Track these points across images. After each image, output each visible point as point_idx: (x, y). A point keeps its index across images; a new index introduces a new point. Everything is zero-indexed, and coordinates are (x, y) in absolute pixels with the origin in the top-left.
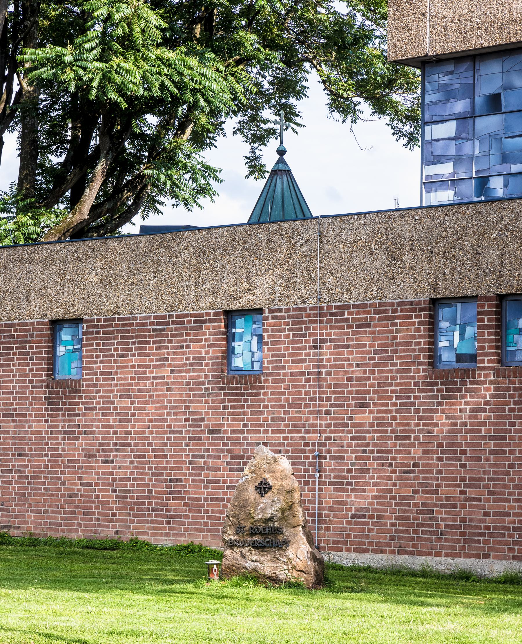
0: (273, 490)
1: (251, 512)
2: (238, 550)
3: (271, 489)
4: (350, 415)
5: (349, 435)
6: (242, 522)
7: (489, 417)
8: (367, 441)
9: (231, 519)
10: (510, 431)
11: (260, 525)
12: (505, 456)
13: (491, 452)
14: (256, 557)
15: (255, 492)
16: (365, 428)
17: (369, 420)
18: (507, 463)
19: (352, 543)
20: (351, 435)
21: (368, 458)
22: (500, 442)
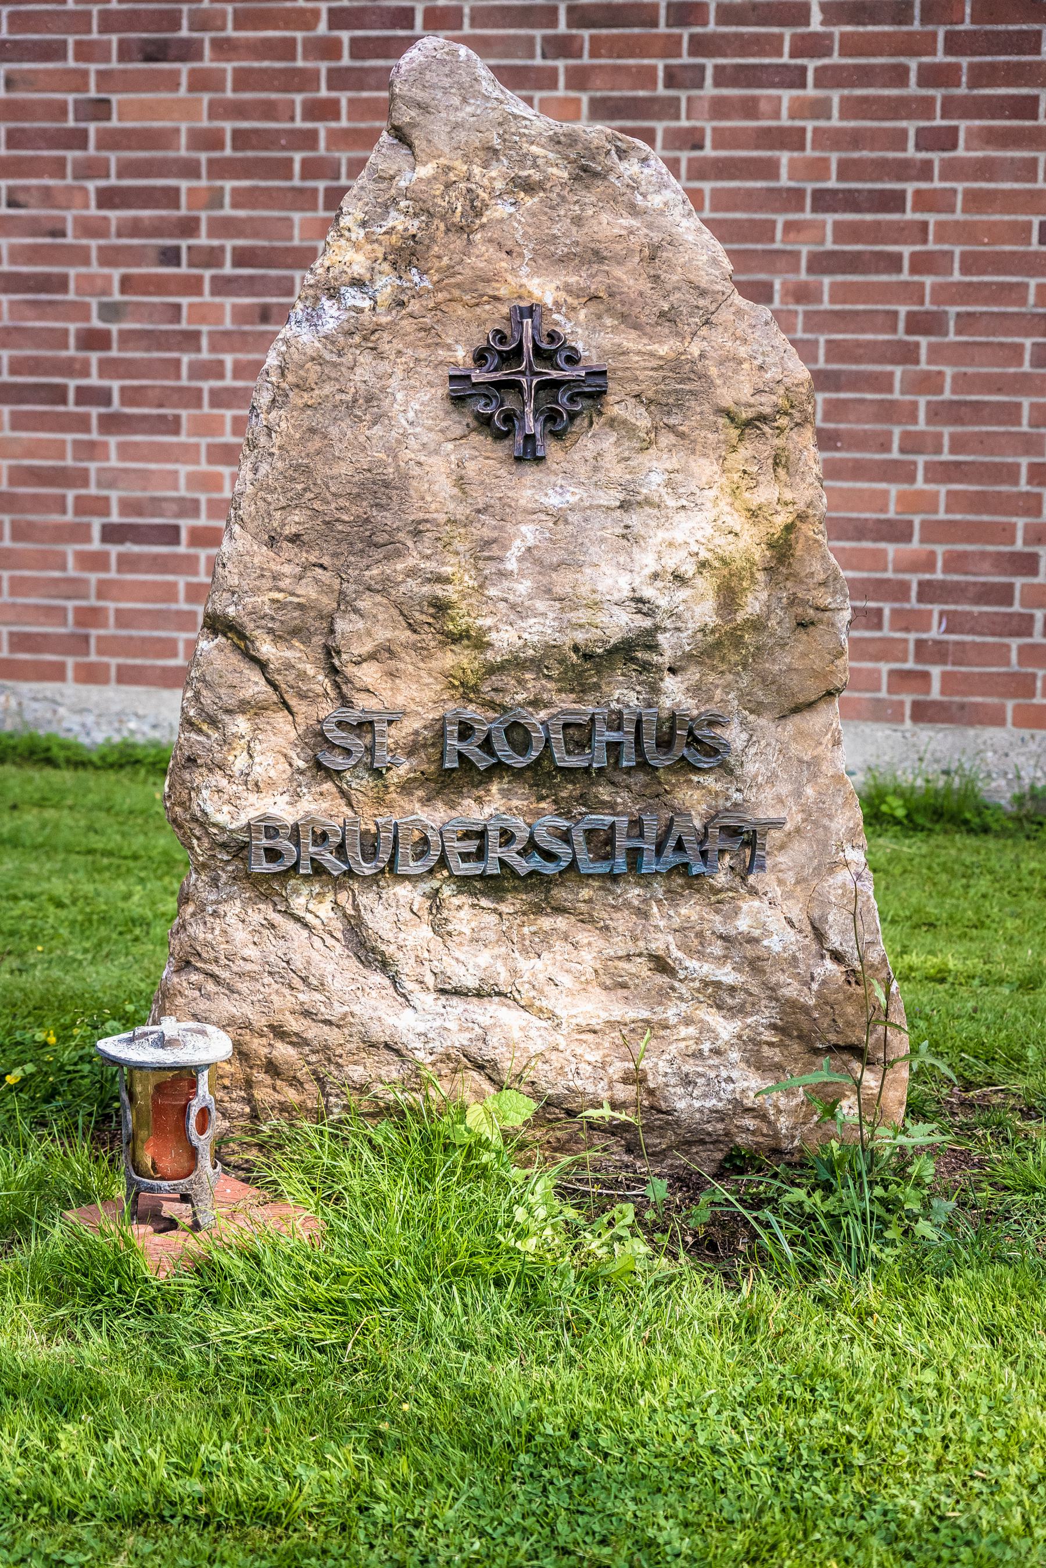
0: (614, 411)
1: (450, 592)
2: (325, 910)
3: (598, 395)
4: (93, 94)
5: (91, 185)
6: (368, 674)
7: (819, 109)
8: (183, 212)
9: (266, 648)
10: (925, 171)
11: (536, 703)
12: (894, 278)
13: (821, 263)
14: (484, 958)
15: (457, 423)
16: (171, 154)
17: (192, 114)
18: (903, 310)
19: (107, 646)
20: (102, 183)
21: (193, 286)
22: (869, 217)
